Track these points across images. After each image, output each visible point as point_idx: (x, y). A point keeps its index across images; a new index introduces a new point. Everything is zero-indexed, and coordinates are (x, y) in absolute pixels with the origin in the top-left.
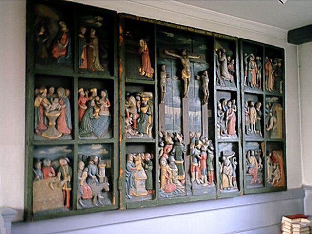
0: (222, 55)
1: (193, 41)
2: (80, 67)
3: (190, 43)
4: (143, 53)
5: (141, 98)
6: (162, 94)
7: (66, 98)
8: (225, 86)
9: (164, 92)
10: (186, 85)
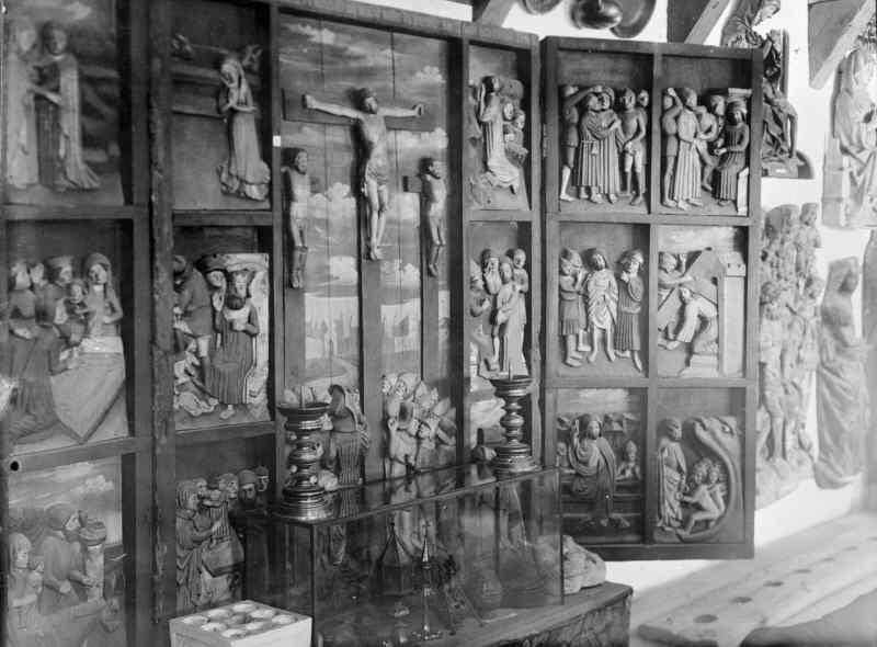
0: (487, 100)
1: (396, 54)
2: (754, 28)
3: (389, 63)
4: (233, 112)
5: (229, 277)
6: (297, 254)
7: (6, 389)
8: (847, 215)
9: (304, 248)
10: (375, 215)
